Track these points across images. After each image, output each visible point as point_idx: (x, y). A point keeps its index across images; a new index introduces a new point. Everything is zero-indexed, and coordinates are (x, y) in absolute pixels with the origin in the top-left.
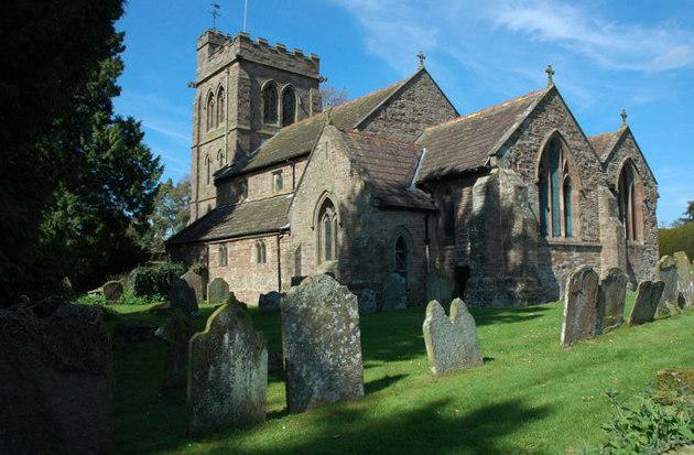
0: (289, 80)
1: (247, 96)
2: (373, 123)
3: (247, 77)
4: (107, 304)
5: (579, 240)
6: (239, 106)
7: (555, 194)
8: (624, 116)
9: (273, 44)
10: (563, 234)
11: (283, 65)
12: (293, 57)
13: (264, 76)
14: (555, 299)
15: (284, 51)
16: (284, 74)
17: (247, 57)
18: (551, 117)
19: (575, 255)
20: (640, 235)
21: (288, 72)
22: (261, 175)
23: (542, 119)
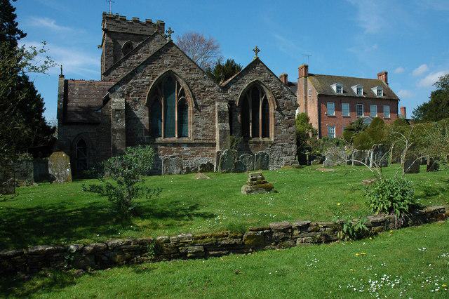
0: (141, 40)
1: (111, 53)
2: (115, 71)
3: (111, 41)
4: (23, 290)
5: (191, 139)
6: (106, 59)
7: (168, 110)
8: (257, 51)
9: (143, 20)
10: (176, 136)
11: (137, 31)
12: (145, 25)
13: (123, 39)
14: (77, 175)
15: (151, 23)
16: (139, 36)
17: (111, 29)
18: (167, 62)
19: (185, 149)
20: (272, 134)
21: (140, 35)
22: (316, 105)
23: (157, 64)
